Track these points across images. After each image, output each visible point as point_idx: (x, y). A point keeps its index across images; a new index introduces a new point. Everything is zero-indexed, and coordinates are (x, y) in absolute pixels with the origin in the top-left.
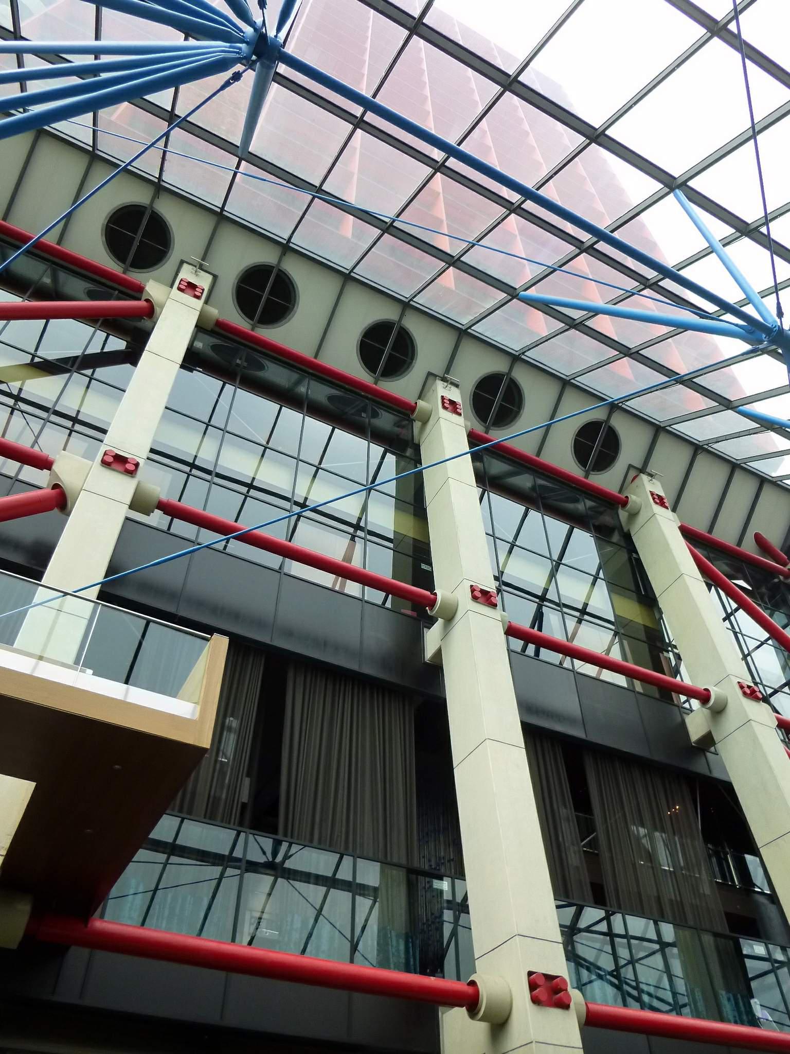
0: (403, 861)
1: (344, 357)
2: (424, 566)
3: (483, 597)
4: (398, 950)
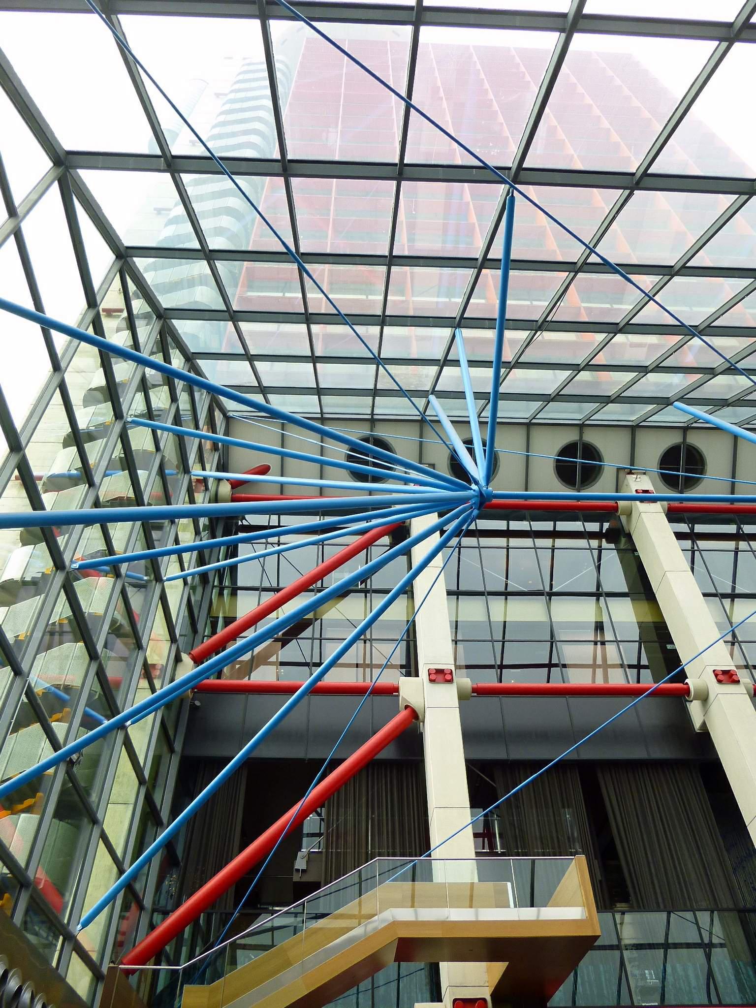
1: (548, 485)
2: (669, 647)
3: (726, 677)
4: (749, 976)
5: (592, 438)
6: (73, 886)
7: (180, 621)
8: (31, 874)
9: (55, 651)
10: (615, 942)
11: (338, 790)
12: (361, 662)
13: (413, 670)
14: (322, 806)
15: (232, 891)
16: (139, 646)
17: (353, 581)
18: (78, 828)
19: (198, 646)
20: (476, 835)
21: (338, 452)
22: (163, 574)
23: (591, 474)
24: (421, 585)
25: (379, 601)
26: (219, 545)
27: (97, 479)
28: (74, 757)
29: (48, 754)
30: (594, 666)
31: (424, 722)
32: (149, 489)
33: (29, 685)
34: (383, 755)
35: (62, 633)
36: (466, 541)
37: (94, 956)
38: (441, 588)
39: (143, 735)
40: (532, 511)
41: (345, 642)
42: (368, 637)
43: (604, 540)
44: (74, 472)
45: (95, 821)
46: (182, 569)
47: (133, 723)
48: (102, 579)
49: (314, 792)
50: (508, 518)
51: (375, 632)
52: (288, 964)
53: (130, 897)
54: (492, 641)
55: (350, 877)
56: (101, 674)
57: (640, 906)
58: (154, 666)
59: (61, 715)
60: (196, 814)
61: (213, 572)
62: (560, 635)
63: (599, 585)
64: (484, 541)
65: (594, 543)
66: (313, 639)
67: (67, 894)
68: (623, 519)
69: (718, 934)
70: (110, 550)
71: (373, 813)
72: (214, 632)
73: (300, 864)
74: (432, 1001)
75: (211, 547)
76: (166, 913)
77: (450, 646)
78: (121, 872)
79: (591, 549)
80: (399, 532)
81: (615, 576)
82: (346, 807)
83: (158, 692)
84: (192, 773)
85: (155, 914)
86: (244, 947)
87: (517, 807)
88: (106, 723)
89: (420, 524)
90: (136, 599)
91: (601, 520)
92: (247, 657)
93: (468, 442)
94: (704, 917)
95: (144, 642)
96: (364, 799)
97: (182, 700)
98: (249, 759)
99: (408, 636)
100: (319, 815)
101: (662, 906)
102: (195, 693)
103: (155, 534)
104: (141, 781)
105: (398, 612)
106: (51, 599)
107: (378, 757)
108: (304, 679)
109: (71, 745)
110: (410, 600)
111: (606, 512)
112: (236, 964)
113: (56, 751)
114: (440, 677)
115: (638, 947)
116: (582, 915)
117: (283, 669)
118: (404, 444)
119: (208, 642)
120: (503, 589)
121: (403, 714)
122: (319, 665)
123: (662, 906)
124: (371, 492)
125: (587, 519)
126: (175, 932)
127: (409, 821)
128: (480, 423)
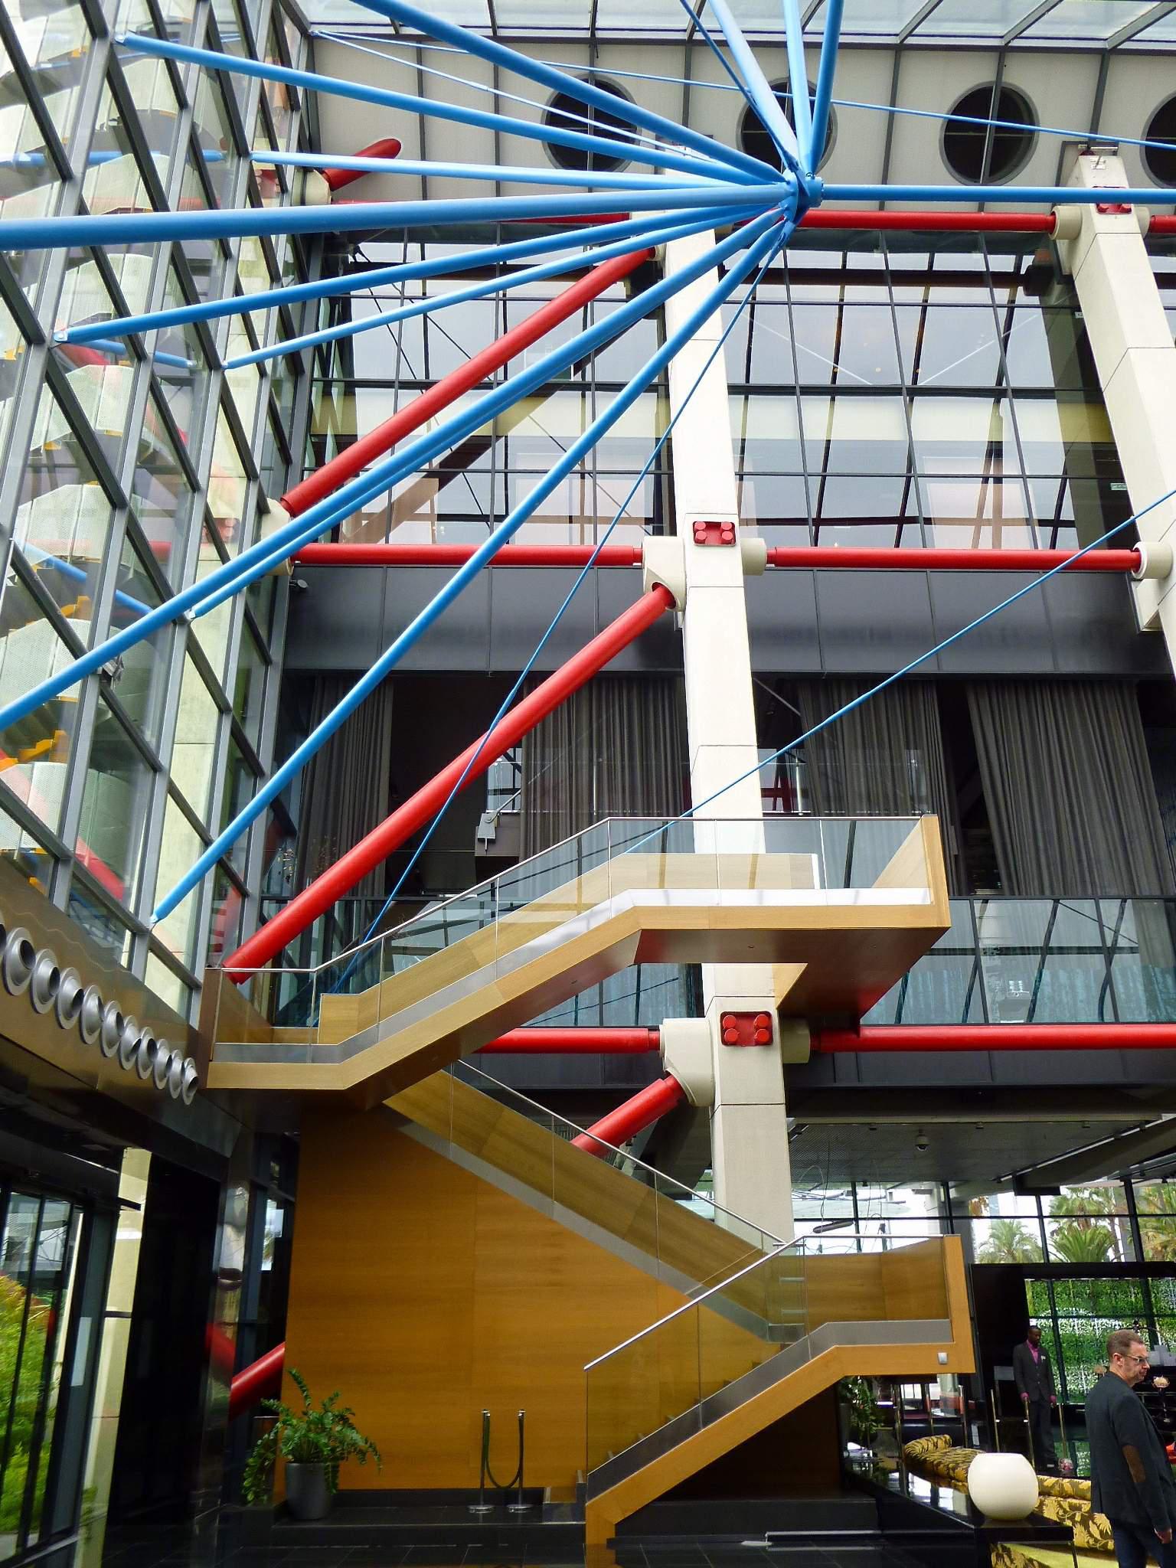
0: (1157, 893)
1: (925, 173)
2: (1115, 487)
4: (1166, 987)
5: (1021, 77)
6: (135, 853)
7: (259, 442)
8: (67, 842)
9: (46, 500)
10: (970, 945)
11: (543, 718)
12: (576, 513)
13: (666, 525)
14: (517, 744)
15: (380, 870)
16: (195, 487)
17: (557, 365)
18: (130, 782)
19: (295, 486)
20: (766, 793)
21: (529, 103)
22: (221, 357)
23: (1011, 152)
24: (682, 371)
25: (607, 403)
26: (317, 294)
27: (76, 165)
28: (109, 667)
29: (63, 662)
30: (978, 522)
31: (684, 611)
32: (175, 187)
33: (16, 550)
34: (615, 665)
35: (53, 468)
36: (765, 291)
37: (182, 958)
38: (718, 379)
39: (217, 632)
40: (890, 232)
41: (546, 478)
42: (589, 467)
43: (1020, 289)
44: (25, 158)
45: (156, 768)
46: (254, 346)
47: (201, 613)
48: (112, 370)
49: (503, 724)
50: (843, 246)
51: (602, 458)
52: (474, 965)
53: (226, 881)
54: (805, 475)
55: (564, 849)
56: (134, 533)
57: (1016, 891)
58: (222, 521)
59: (74, 607)
60: (315, 756)
61: (311, 349)
62: (923, 466)
63: (1002, 374)
64: (799, 291)
65: (1002, 295)
66: (493, 471)
67: (127, 878)
68: (1062, 246)
69: (1129, 932)
70: (121, 309)
71: (599, 755)
72: (320, 461)
73: (485, 830)
74: (689, 1015)
75: (302, 298)
76: (281, 901)
77: (732, 481)
78: (207, 842)
79: (994, 306)
80: (643, 270)
81: (1033, 360)
82: (556, 746)
83: (235, 558)
84: (304, 694)
85: (266, 902)
86: (404, 950)
87: (833, 747)
88: (152, 614)
89: (681, 253)
90: (178, 404)
91: (1017, 248)
92: (377, 505)
93: (781, 87)
94: (1110, 908)
95: (201, 478)
96: (585, 735)
97: (276, 579)
98: (392, 672)
99: (658, 466)
100: (509, 758)
101: (1047, 892)
102: (296, 566)
103: (200, 283)
104: (223, 709)
105: (639, 421)
106: (28, 398)
107: (605, 668)
108: (480, 540)
109: (99, 648)
110: (663, 401)
111: (1033, 235)
112: (392, 970)
113: (76, 657)
114: (713, 535)
115: (1003, 951)
116: (924, 899)
117: (443, 526)
118: (649, 88)
119: (311, 479)
120: (827, 381)
121: (649, 598)
122: (500, 518)
123: (1047, 892)
124: (591, 187)
125: (994, 248)
126: (299, 926)
127: (658, 766)
128: (807, 45)
